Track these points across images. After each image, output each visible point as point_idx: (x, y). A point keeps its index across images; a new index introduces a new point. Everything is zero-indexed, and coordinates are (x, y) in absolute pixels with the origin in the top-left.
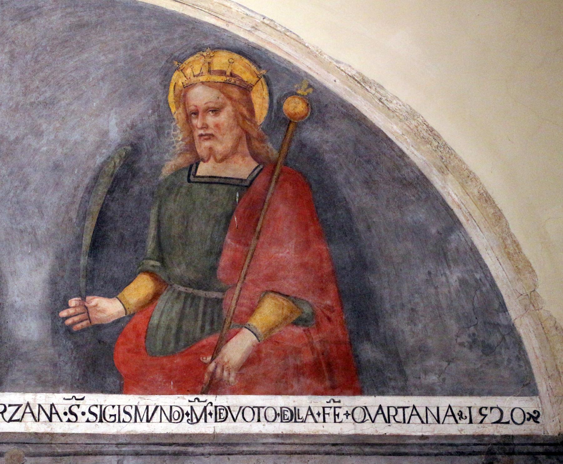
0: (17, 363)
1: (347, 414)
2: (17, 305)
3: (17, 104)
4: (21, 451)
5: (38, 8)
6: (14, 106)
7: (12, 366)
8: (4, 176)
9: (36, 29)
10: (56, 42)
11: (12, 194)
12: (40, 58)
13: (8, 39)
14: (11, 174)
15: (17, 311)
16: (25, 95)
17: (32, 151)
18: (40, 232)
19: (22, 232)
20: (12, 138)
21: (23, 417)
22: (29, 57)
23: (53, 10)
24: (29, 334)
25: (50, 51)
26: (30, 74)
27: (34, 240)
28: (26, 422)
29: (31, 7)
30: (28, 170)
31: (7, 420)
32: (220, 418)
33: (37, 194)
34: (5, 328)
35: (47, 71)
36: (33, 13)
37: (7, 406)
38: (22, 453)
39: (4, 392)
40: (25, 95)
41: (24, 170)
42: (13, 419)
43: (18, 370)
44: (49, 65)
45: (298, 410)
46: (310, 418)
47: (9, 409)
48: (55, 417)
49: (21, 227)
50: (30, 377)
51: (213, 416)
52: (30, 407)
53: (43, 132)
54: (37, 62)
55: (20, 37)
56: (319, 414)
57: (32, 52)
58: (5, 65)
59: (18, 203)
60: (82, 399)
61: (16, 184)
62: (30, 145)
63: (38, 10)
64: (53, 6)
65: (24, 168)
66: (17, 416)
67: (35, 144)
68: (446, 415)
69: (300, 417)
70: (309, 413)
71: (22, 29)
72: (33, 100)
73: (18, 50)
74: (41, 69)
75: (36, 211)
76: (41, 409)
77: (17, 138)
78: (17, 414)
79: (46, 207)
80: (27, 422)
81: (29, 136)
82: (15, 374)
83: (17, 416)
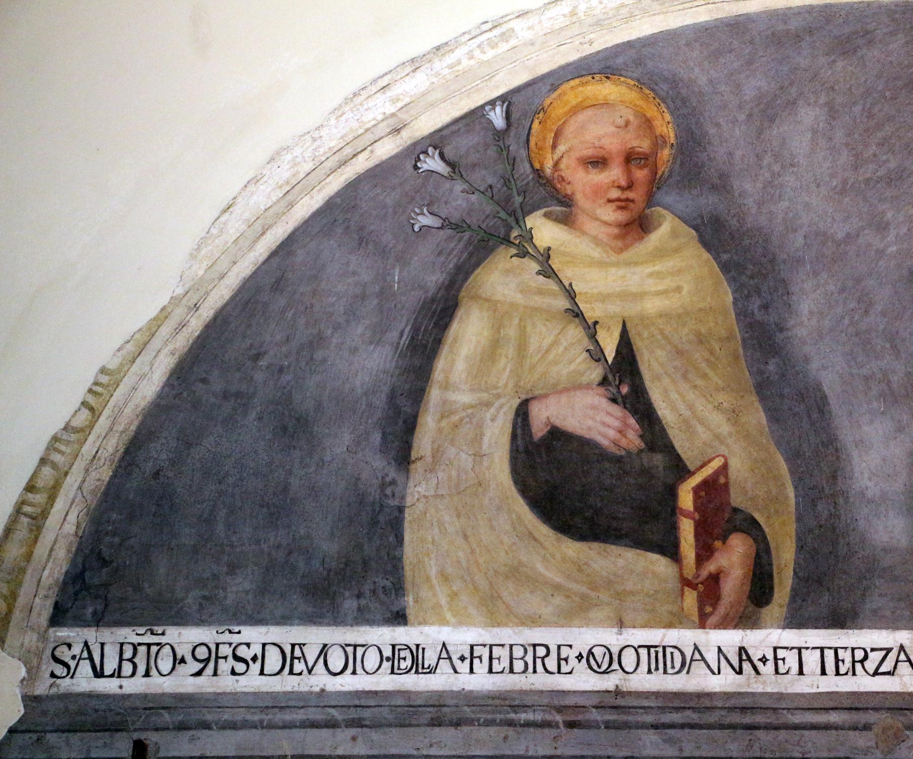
0: (877, 583)
1: (580, 657)
2: (869, 494)
3: (845, 182)
4: (898, 721)
5: (867, 33)
6: (840, 186)
7: (869, 588)
8: (832, 294)
9: (866, 66)
10: (900, 83)
11: (846, 321)
12: (876, 110)
13: (823, 85)
14: (842, 290)
15: (870, 501)
16: (856, 168)
17: (873, 252)
18: (896, 378)
19: (868, 379)
20: (840, 235)
21: (895, 667)
22: (857, 109)
23: (892, 33)
24: (891, 538)
25: (891, 98)
26: (860, 135)
27: (887, 392)
28: (901, 676)
29: (856, 32)
30: (870, 283)
31: (871, 672)
32: (423, 668)
33: (886, 319)
34: (854, 530)
35: (888, 129)
36: (860, 41)
37: (869, 650)
38: (900, 725)
39: (861, 628)
40: (856, 168)
41: (863, 284)
42: (881, 670)
43: (881, 595)
44: (890, 119)
45: (423, 649)
46: (444, 665)
47: (871, 655)
48: (746, 666)
49: (864, 371)
50: (902, 605)
51: (468, 661)
52: (905, 651)
53: (888, 224)
54: (870, 116)
55: (841, 80)
56: (462, 659)
57: (862, 102)
58: (821, 124)
59: (857, 334)
60: (239, 632)
61: (851, 306)
62: (869, 245)
63: (868, 36)
64: (891, 28)
65: (862, 279)
66: (887, 667)
67: (877, 243)
68: (439, 658)
69: (426, 666)
70: (744, 657)
71: (844, 67)
72: (869, 175)
73: (839, 100)
74: (879, 126)
75: (888, 345)
76: (722, 657)
77: (848, 235)
78: (885, 663)
79: (904, 340)
80: (903, 675)
81: (867, 231)
82: (874, 602)
83: (887, 667)
